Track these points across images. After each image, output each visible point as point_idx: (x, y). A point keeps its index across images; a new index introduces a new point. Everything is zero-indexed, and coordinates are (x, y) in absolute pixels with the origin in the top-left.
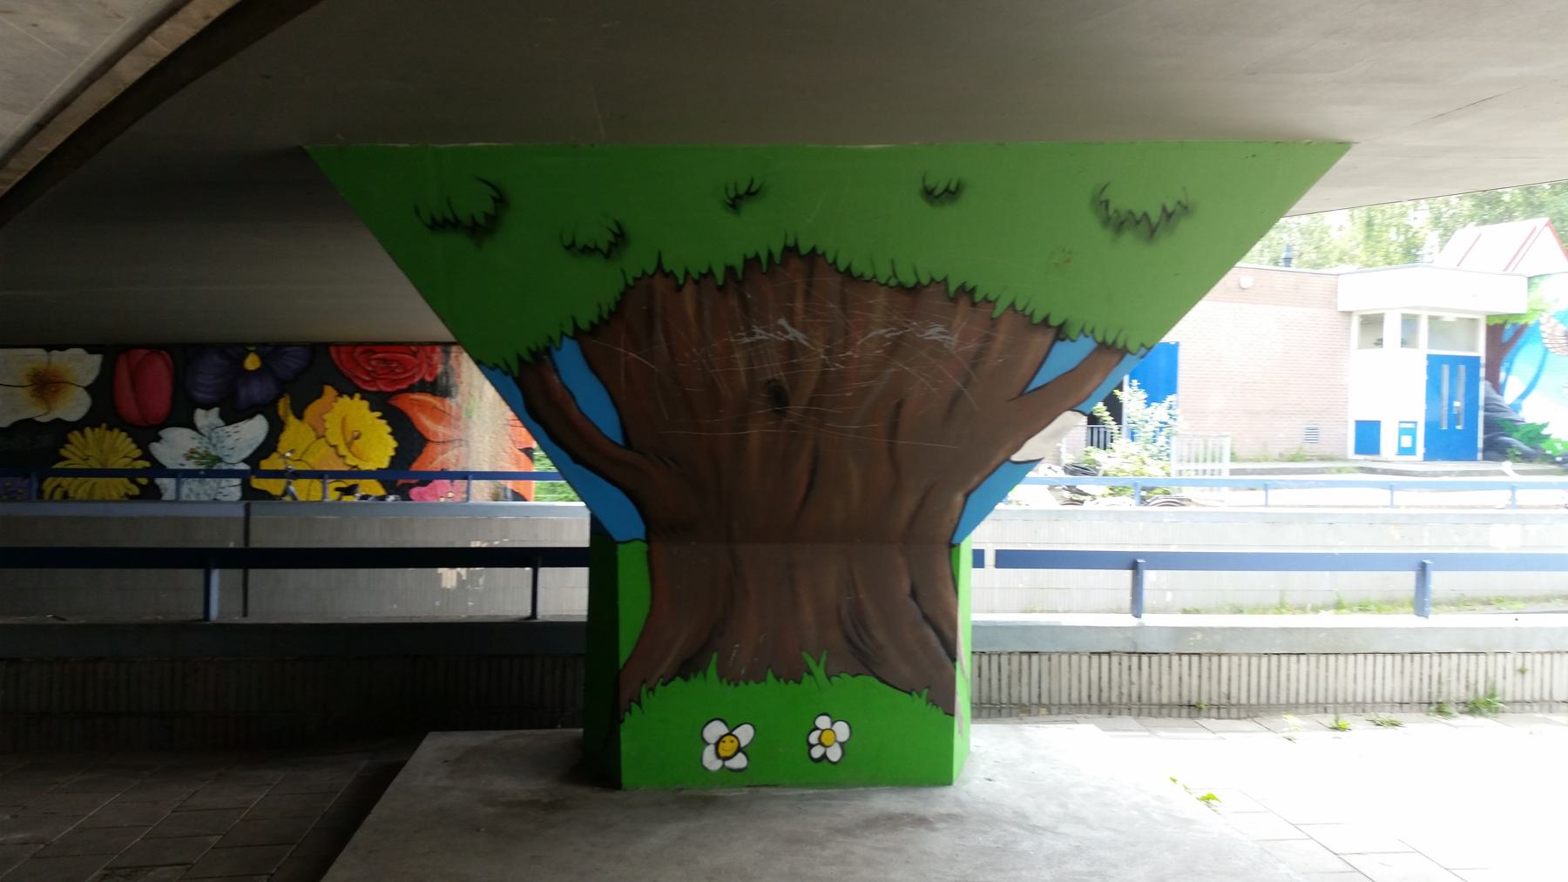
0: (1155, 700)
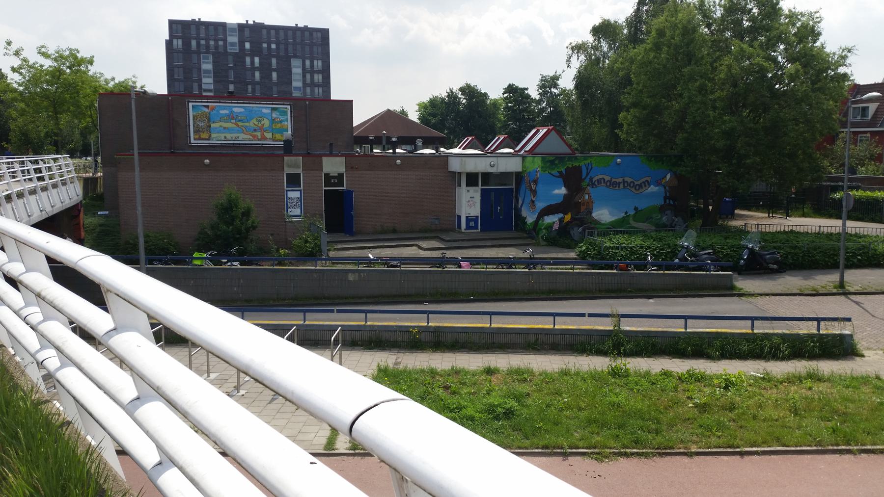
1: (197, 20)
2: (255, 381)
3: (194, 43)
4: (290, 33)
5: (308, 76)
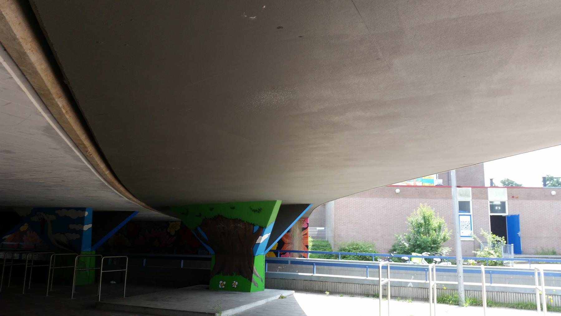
0: (315, 289)
2: (64, 128)
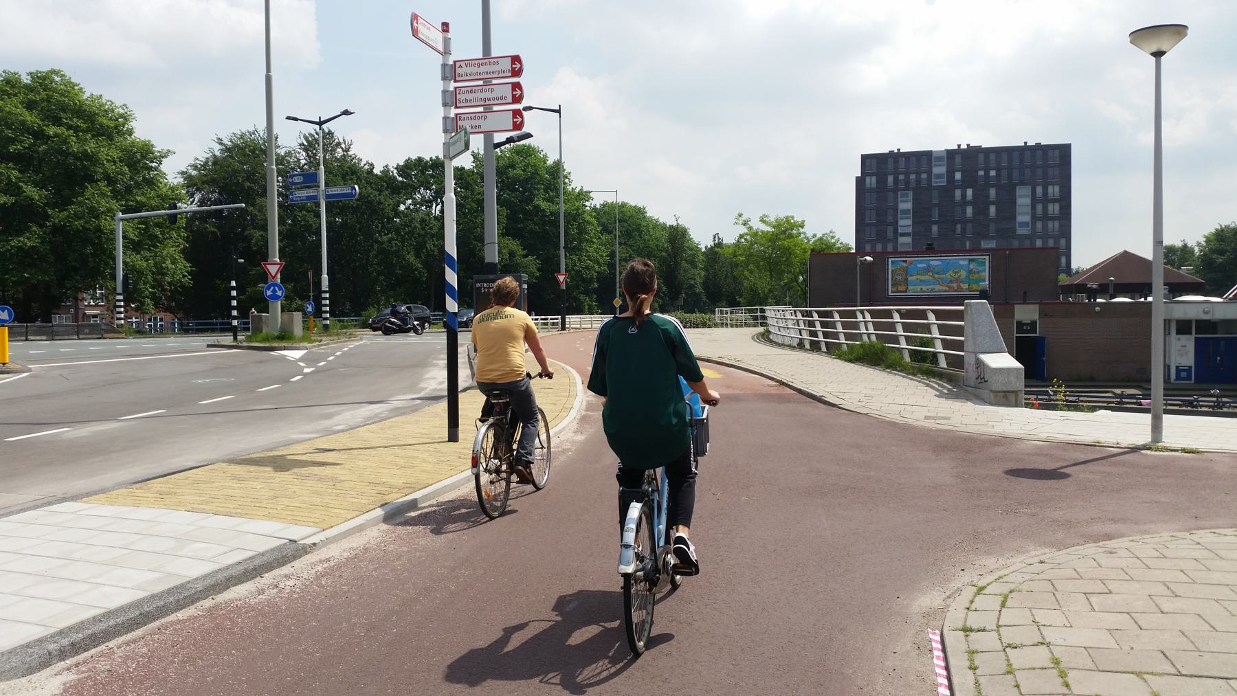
1: (896, 151)
3: (890, 179)
4: (1016, 155)
5: (1039, 207)
